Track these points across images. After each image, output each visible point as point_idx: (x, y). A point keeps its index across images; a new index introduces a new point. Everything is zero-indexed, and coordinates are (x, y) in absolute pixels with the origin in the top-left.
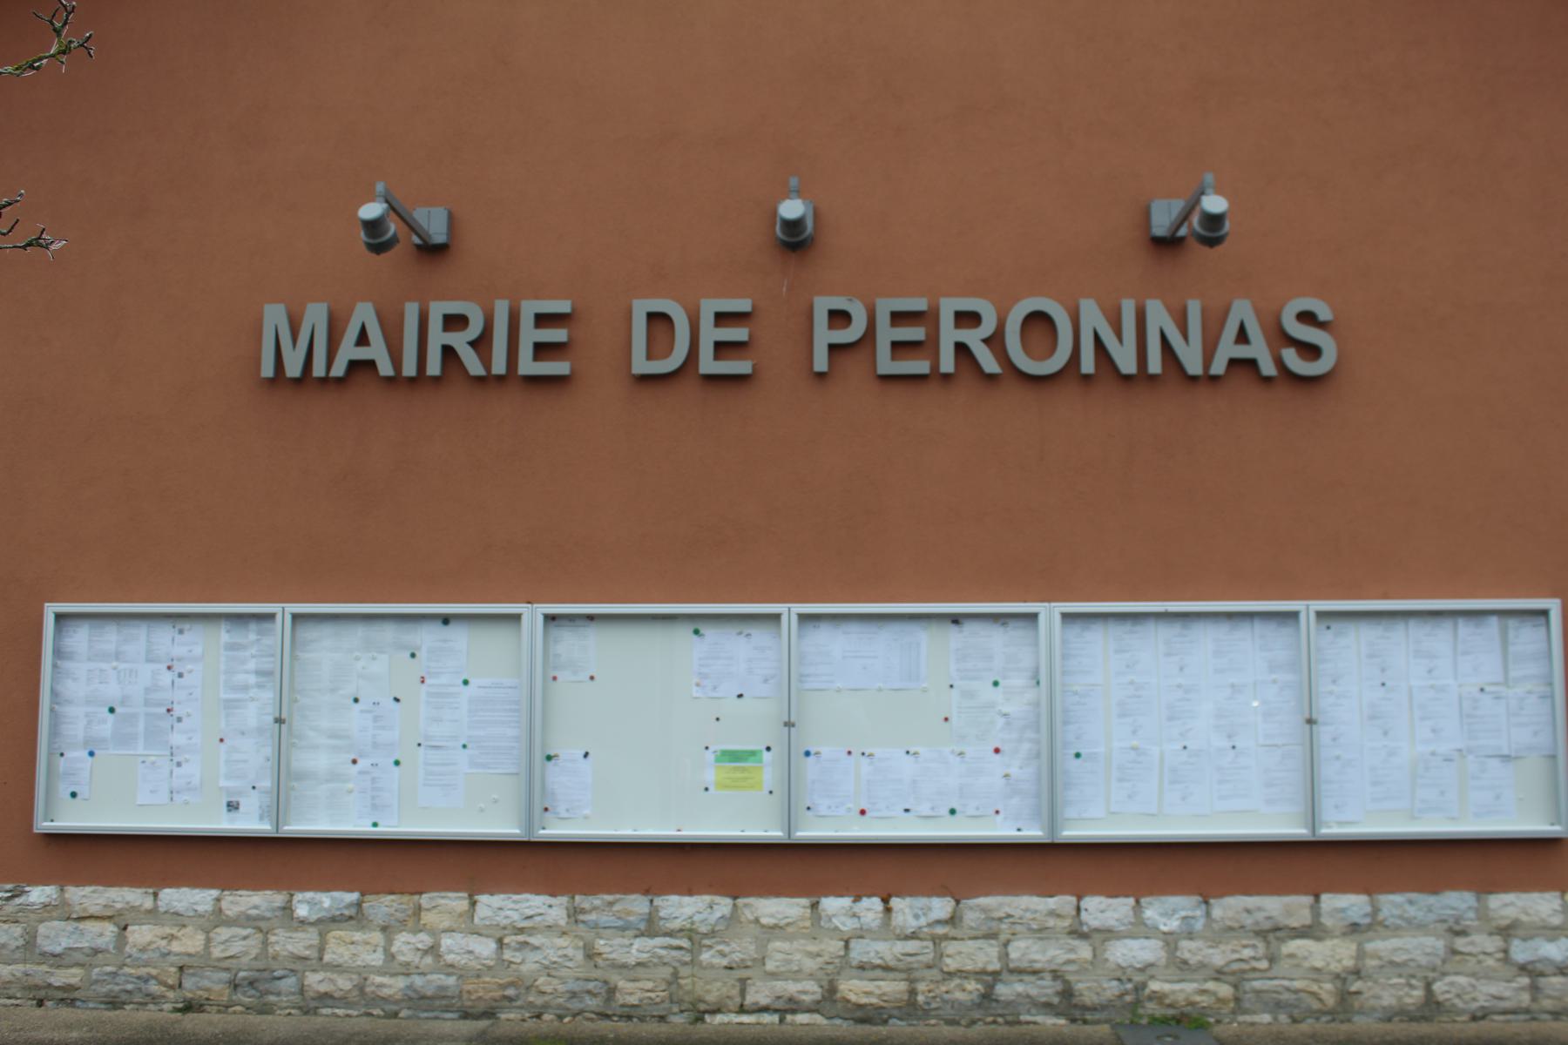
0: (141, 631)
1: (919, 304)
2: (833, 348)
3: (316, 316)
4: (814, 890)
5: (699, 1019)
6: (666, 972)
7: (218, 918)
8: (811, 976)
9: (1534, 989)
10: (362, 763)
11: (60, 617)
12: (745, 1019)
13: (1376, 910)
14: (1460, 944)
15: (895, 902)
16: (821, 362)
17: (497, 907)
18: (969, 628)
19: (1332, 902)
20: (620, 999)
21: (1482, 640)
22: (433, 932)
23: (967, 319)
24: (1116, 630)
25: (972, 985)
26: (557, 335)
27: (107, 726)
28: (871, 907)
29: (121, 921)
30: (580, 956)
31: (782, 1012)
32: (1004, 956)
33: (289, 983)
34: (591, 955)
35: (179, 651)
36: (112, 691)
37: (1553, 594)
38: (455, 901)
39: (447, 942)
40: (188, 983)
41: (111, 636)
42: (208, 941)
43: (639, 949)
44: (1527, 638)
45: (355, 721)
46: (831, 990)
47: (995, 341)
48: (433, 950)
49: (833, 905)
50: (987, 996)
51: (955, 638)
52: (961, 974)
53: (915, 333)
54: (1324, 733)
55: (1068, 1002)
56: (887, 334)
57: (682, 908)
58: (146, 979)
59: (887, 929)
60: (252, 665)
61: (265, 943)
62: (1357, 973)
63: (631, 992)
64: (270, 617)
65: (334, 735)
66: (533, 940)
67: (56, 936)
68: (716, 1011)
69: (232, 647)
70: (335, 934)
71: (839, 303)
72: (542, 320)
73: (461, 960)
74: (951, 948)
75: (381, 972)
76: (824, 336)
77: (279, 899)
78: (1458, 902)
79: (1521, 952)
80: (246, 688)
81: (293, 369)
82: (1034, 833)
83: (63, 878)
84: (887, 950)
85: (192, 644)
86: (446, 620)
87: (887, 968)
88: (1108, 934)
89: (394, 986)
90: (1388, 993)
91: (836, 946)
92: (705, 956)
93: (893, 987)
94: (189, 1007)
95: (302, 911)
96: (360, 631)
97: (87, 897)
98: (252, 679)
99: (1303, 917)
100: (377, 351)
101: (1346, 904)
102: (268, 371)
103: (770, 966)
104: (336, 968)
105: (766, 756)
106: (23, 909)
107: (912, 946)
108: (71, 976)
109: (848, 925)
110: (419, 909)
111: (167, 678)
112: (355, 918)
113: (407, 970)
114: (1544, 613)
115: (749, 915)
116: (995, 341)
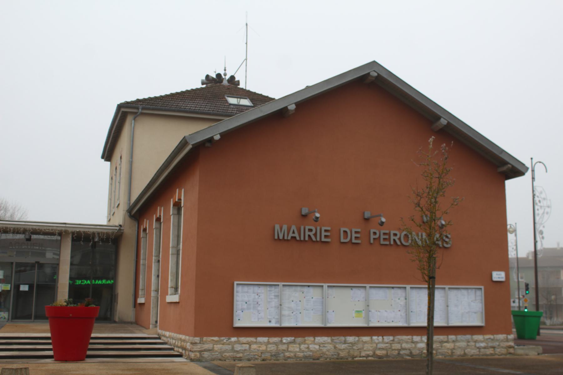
0: (252, 288)
1: (387, 232)
2: (374, 239)
3: (285, 227)
4: (371, 335)
5: (353, 358)
6: (347, 351)
7: (269, 343)
8: (371, 351)
9: (479, 351)
10: (294, 313)
11: (237, 284)
12: (361, 358)
13: (457, 338)
14: (469, 344)
15: (384, 337)
16: (372, 241)
17: (319, 339)
18: (395, 289)
19: (450, 337)
20: (340, 355)
21: (472, 293)
22: (308, 345)
23: (395, 235)
24: (418, 290)
25: (397, 352)
26: (328, 234)
27: (245, 306)
28: (380, 338)
29: (250, 344)
30: (333, 348)
31: (367, 357)
32: (401, 346)
33: (282, 355)
34: (335, 347)
35: (259, 291)
36: (246, 299)
37: (482, 285)
38: (312, 339)
39: (311, 346)
40: (263, 356)
41: (246, 289)
42: (267, 347)
43: (343, 346)
44: (479, 293)
45: (293, 305)
46: (374, 353)
47: (400, 239)
48: (308, 348)
49: (375, 338)
50: (399, 354)
51: (392, 291)
52: (395, 350)
53: (387, 237)
54: (449, 308)
55: (411, 354)
56: (382, 237)
57: (351, 339)
58: (254, 355)
59: (383, 342)
60: (273, 294)
61: (277, 348)
62: (454, 349)
63: (342, 354)
64: (278, 285)
65: (289, 308)
66: (326, 345)
67: (238, 347)
68: (356, 357)
69: (270, 291)
70: (291, 345)
71: (375, 231)
72: (326, 231)
73: (314, 349)
74: (393, 345)
75: (298, 352)
76: (372, 237)
77: (280, 339)
78: (468, 337)
79: (478, 345)
80: (272, 299)
81: (281, 237)
82: (405, 325)
83: (238, 336)
84: (382, 346)
85: (262, 290)
86: (309, 286)
87: (383, 349)
88: (417, 342)
89: (301, 355)
90: (459, 352)
91: (375, 345)
92: (355, 347)
93: (384, 352)
94: (263, 360)
95: (284, 341)
96: (294, 288)
97: (243, 339)
98: (273, 297)
99: (446, 340)
100: (296, 235)
101: (452, 337)
102: (276, 237)
103: (365, 349)
104: (290, 352)
105: (363, 312)
106: (231, 342)
107: (387, 345)
108: (241, 355)
109: (377, 341)
110: (305, 340)
111: (257, 297)
112: (294, 342)
113: (303, 352)
114: (481, 289)
115: (361, 340)
116: (400, 239)
